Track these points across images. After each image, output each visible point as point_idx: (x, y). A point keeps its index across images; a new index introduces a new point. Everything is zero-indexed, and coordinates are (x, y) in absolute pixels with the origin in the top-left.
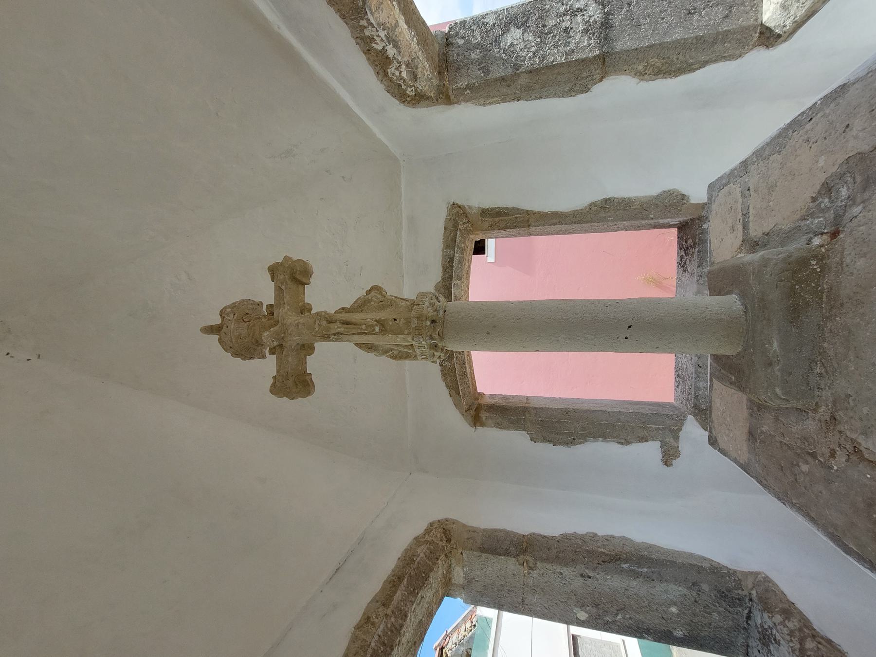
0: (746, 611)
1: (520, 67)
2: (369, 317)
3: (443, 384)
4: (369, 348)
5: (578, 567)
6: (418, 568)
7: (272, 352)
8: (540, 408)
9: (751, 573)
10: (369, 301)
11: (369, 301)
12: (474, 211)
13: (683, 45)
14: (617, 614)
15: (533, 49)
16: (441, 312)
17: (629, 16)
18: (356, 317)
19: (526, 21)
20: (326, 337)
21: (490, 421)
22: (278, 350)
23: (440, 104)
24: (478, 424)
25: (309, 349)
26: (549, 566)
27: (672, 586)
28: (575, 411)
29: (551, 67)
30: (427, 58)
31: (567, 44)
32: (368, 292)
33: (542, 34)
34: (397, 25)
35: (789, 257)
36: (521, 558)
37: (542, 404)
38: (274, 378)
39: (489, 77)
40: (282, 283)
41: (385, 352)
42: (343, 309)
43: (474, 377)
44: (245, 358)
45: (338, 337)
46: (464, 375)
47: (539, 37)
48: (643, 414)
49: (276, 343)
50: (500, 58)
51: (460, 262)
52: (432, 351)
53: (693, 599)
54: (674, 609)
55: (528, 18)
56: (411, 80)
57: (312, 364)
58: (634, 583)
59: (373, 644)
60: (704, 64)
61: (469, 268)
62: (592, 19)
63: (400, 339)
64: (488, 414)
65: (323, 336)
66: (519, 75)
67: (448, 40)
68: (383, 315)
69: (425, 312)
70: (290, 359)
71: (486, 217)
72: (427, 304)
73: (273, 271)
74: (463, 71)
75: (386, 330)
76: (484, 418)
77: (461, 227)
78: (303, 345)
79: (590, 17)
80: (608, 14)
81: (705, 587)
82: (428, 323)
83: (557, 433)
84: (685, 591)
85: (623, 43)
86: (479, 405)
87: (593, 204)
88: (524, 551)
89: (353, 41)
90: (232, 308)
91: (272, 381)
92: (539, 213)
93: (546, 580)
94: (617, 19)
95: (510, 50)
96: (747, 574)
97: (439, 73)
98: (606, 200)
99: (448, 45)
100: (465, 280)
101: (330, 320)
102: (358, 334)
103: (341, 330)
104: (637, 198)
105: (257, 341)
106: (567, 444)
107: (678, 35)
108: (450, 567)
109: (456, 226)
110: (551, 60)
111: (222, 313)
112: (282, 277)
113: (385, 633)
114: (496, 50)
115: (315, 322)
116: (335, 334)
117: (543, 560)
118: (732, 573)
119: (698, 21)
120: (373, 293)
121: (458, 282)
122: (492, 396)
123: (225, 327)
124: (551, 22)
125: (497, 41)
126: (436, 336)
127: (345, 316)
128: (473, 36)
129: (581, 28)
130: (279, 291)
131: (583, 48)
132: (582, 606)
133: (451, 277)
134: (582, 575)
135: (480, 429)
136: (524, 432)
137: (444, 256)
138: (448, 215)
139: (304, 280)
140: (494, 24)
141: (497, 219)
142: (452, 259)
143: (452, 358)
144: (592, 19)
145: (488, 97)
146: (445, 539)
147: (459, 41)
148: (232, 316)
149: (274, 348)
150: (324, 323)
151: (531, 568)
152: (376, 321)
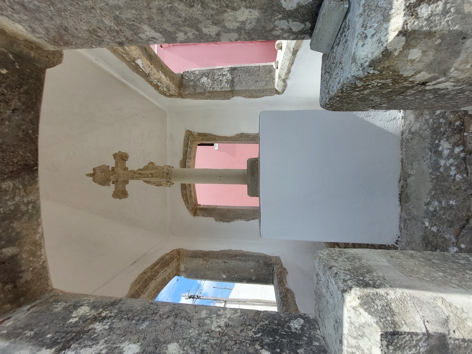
0: (272, 268)
1: (206, 90)
2: (148, 172)
3: (182, 200)
4: (148, 182)
5: (223, 259)
6: (166, 261)
7: (113, 183)
8: (219, 209)
9: (275, 257)
10: (149, 167)
11: (149, 167)
12: (196, 134)
13: (254, 91)
14: (235, 275)
15: (210, 85)
16: (170, 171)
17: (239, 80)
18: (143, 172)
19: (208, 75)
20: (133, 178)
21: (200, 214)
22: (115, 182)
23: (180, 98)
24: (196, 215)
25: (127, 182)
26: (213, 260)
27: (251, 262)
28: (231, 210)
29: (216, 92)
30: (174, 84)
31: (221, 85)
32: (149, 164)
33: (214, 80)
34: (161, 78)
35: (252, 160)
36: (204, 258)
37: (221, 208)
38: (114, 192)
39: (196, 92)
40: (118, 160)
41: (154, 184)
42: (139, 169)
43: (196, 198)
44: (103, 185)
45: (137, 178)
46: (191, 196)
47: (212, 81)
48: (254, 210)
49: (115, 180)
50: (200, 86)
51: (190, 153)
52: (167, 183)
53: (257, 266)
54: (252, 270)
55: (209, 74)
56: (168, 91)
57: (128, 188)
58: (240, 263)
59: (146, 277)
60: (263, 96)
61: (195, 154)
62: (228, 79)
63: (158, 179)
64: (200, 211)
65: (132, 178)
66: (206, 93)
67: (182, 76)
68: (152, 172)
69: (165, 171)
70: (120, 185)
71: (200, 136)
72: (166, 169)
73: (115, 156)
74: (187, 88)
75: (153, 176)
76: (198, 213)
77: (190, 139)
78: (125, 181)
79: (228, 78)
80: (233, 78)
81: (261, 262)
82: (166, 174)
83: (225, 218)
84: (255, 264)
85: (237, 88)
86: (197, 208)
87: (237, 135)
88: (205, 256)
89: (146, 82)
90: (99, 168)
91: (113, 193)
92: (219, 136)
93: (213, 265)
94: (236, 80)
95: (203, 84)
96: (274, 257)
97: (179, 88)
98: (242, 134)
99: (182, 78)
100: (193, 160)
101: (134, 172)
102: (144, 177)
103: (138, 176)
104: (251, 134)
105: (108, 179)
106: (228, 222)
107: (253, 88)
108: (179, 264)
109: (188, 139)
110: (216, 89)
111: (94, 169)
112: (118, 158)
113: (150, 276)
114: (199, 83)
115: (129, 173)
116: (136, 177)
117: (211, 258)
118: (270, 257)
119: (258, 85)
120: (150, 165)
121: (189, 160)
122: (204, 205)
123: (96, 174)
124: (216, 77)
125: (199, 80)
126: (168, 178)
127: (140, 172)
128: (191, 77)
129: (225, 81)
130: (117, 163)
131: (226, 87)
132: (224, 273)
133: (186, 158)
134: (224, 262)
135: (196, 217)
136: (213, 218)
137: (184, 150)
138: (186, 134)
139: (126, 159)
140: (198, 74)
141: (204, 137)
142: (187, 151)
143: (186, 189)
144: (228, 79)
145: (196, 98)
146: (178, 254)
147: (186, 78)
148: (99, 170)
149: (114, 182)
150: (132, 174)
151: (208, 262)
152: (150, 173)
